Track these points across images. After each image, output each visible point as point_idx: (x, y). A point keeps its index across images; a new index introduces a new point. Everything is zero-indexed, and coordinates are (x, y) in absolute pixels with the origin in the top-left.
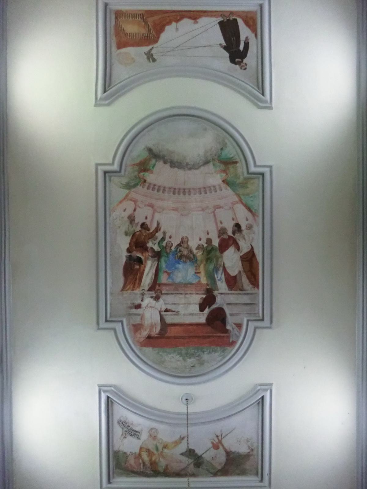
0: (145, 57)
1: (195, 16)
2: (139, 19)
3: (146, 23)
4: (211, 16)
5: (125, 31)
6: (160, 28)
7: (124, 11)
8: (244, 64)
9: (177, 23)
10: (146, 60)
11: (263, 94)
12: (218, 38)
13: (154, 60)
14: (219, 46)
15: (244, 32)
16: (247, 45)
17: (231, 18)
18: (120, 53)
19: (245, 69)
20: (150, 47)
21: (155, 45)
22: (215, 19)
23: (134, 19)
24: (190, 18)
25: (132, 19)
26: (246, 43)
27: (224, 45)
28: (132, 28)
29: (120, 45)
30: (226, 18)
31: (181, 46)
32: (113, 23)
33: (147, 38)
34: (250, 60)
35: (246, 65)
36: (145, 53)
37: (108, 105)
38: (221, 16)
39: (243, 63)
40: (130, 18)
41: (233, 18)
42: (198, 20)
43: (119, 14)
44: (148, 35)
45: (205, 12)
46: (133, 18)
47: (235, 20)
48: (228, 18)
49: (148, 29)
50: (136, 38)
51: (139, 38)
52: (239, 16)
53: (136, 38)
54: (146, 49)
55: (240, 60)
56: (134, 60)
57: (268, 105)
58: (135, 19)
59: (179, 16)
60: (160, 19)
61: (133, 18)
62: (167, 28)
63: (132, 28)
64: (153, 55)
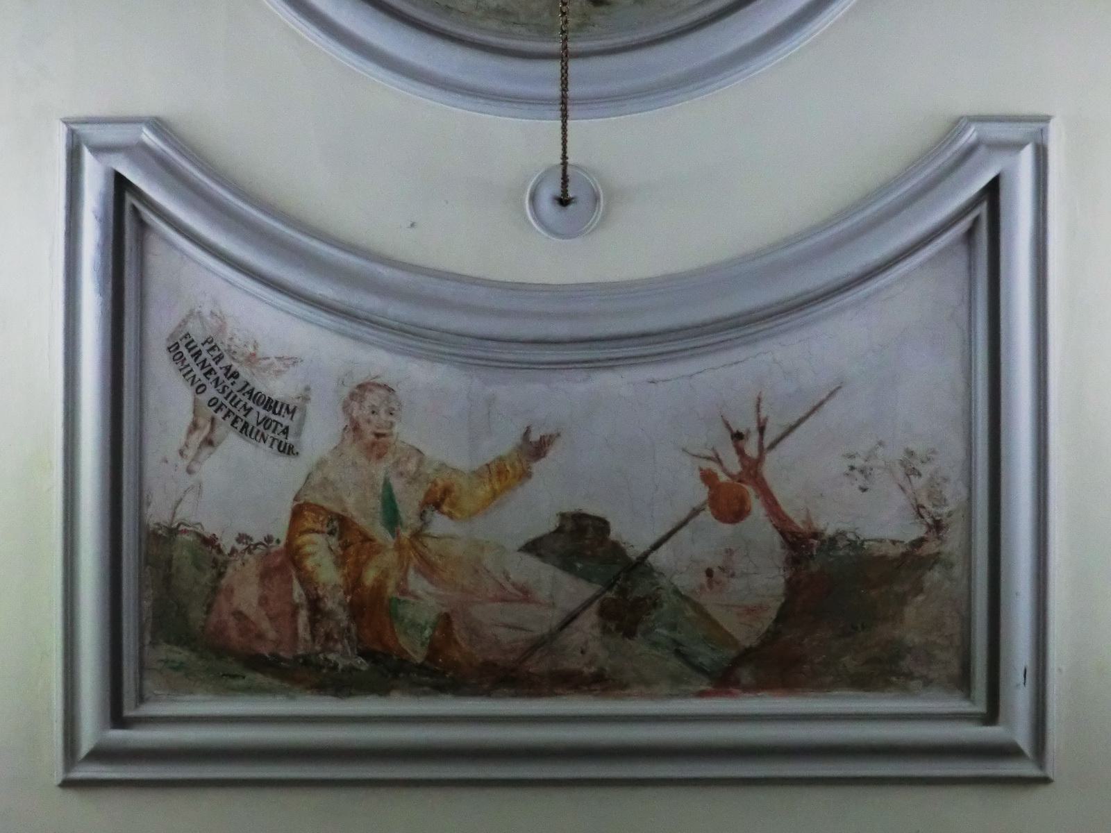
11: (120, 184)
37: (958, 125)
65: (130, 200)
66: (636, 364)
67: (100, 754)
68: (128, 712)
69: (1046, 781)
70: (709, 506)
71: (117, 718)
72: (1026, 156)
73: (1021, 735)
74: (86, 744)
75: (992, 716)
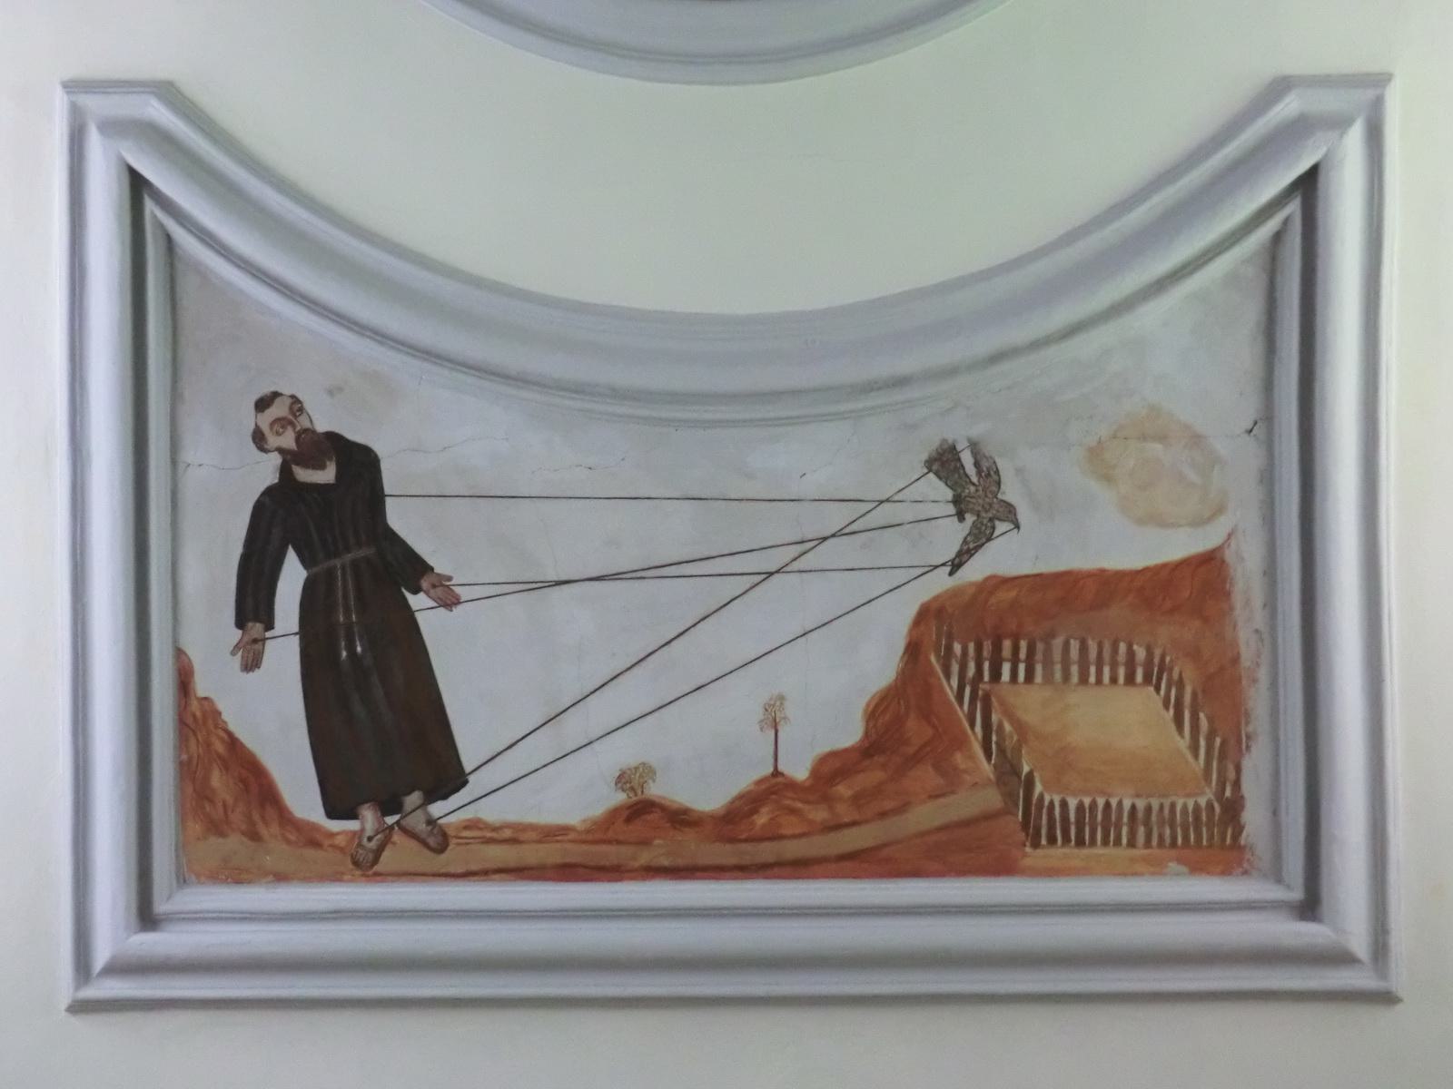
0: (1011, 491)
1: (641, 837)
2: (1064, 804)
3: (1008, 771)
4: (515, 835)
5: (1166, 705)
6: (903, 728)
7: (1173, 866)
8: (273, 441)
9: (776, 773)
10: (1002, 464)
11: (137, 185)
12: (479, 664)
13: (944, 462)
14: (457, 590)
15: (269, 709)
16: (253, 603)
17: (369, 817)
18: (1199, 522)
19: (262, 404)
20: (975, 571)
21: (940, 583)
22: (493, 811)
23: (1101, 802)
24: (680, 818)
25: (1114, 802)
26: (257, 619)
27: (421, 595)
28: (1113, 724)
29: (1198, 585)
30: (417, 822)
31: (747, 582)
32: (1255, 767)
33: (997, 648)
34: (227, 480)
35: (259, 438)
36: (1017, 527)
37: (1280, 87)
38: (439, 840)
39: (280, 450)
40: (1127, 804)
41: (352, 825)
42: (620, 798)
43: (1214, 838)
44: (996, 675)
45: (567, 872)
46: (1108, 805)
47: (335, 809)
48: (390, 820)
49: (995, 718)
50: (1084, 649)
51: (1058, 643)
52: (310, 837)
53: (1084, 649)
54: (1006, 557)
55: (304, 475)
56: (1098, 460)
57: (96, 105)
58: (1094, 805)
59: (758, 832)
60: (902, 809)
61: (1108, 805)
62: (850, 734)
63: (1113, 724)
64: (951, 509)
65: (150, 206)
66: (1205, 255)
67: (121, 968)
68: (161, 906)
69: (1387, 998)
70: (992, 643)
71: (147, 917)
72: (1354, 139)
73: (1359, 943)
74: (102, 954)
75: (1310, 907)
